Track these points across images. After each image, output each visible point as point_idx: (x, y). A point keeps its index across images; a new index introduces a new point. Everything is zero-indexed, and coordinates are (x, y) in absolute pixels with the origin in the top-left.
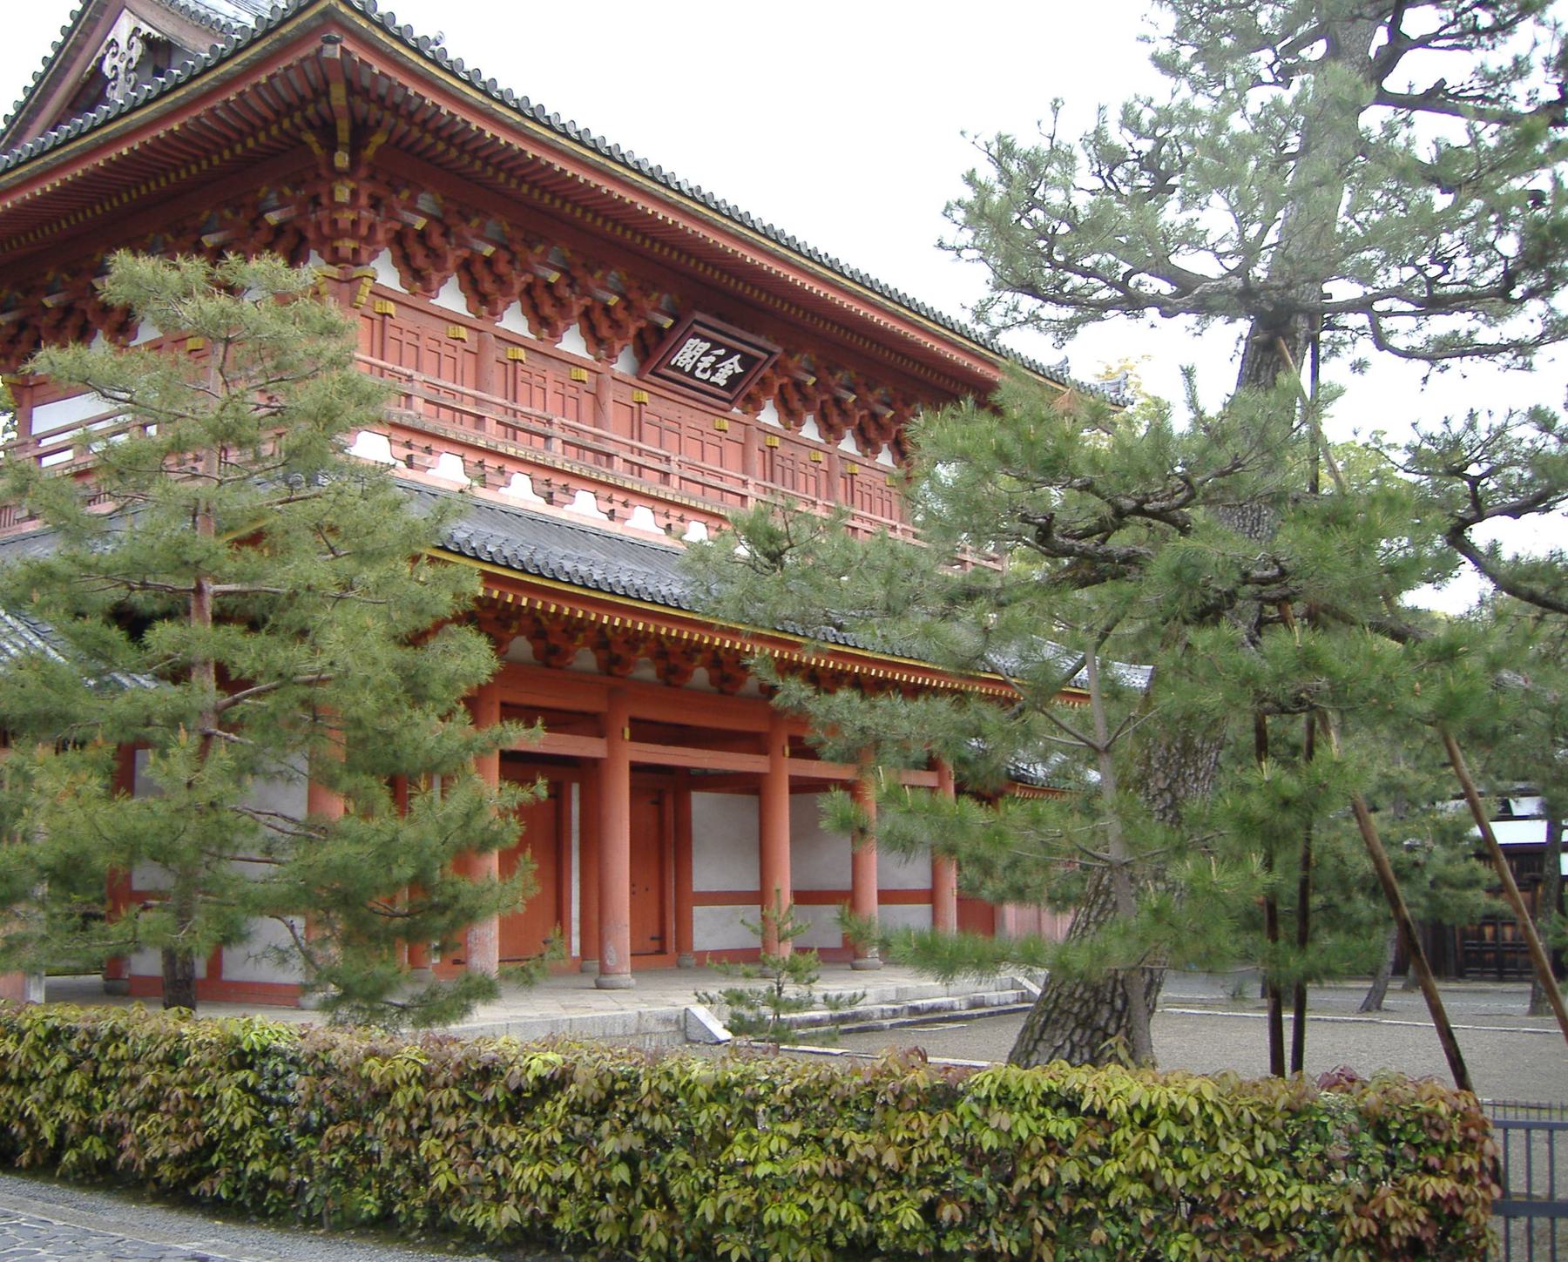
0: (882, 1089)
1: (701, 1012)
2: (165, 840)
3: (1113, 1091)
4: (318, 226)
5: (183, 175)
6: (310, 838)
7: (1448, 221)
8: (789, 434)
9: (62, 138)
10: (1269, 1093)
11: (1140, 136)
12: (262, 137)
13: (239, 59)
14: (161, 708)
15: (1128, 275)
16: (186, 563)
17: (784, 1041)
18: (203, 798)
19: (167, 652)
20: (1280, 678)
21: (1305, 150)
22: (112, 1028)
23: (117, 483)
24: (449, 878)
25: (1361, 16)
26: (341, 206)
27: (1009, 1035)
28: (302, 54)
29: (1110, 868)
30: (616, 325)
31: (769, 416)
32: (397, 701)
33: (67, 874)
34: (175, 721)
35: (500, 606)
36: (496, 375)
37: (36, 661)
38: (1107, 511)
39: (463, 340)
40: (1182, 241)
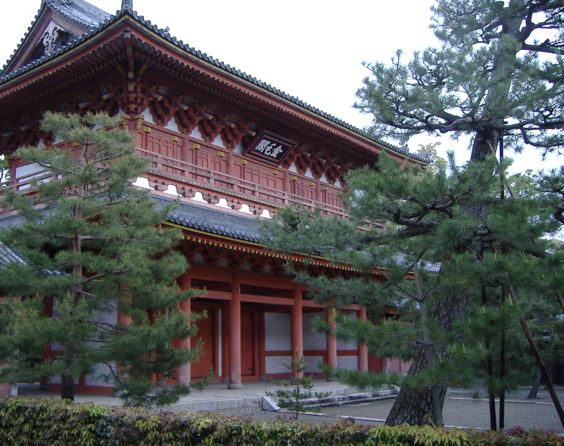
0: (336, 434)
1: (268, 399)
2: (62, 334)
3: (426, 436)
4: (122, 99)
5: (72, 81)
6: (117, 333)
7: (552, 93)
8: (301, 175)
9: (28, 68)
10: (489, 437)
11: (431, 64)
12: (101, 67)
13: (93, 39)
14: (61, 283)
15: (428, 117)
16: (71, 229)
17: (300, 410)
18: (76, 318)
19: (63, 262)
20: (489, 273)
21: (495, 68)
22: (41, 406)
23: (46, 198)
24: (170, 348)
25: (515, 16)
26: (130, 92)
27: (387, 408)
28: (116, 37)
29: (424, 346)
30: (235, 135)
31: (293, 169)
32: (150, 281)
33: (25, 346)
34: (67, 288)
35: (190, 243)
36: (189, 155)
37: (15, 265)
38: (421, 208)
39: (176, 142)
40: (448, 104)
